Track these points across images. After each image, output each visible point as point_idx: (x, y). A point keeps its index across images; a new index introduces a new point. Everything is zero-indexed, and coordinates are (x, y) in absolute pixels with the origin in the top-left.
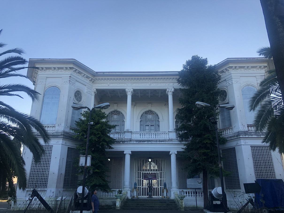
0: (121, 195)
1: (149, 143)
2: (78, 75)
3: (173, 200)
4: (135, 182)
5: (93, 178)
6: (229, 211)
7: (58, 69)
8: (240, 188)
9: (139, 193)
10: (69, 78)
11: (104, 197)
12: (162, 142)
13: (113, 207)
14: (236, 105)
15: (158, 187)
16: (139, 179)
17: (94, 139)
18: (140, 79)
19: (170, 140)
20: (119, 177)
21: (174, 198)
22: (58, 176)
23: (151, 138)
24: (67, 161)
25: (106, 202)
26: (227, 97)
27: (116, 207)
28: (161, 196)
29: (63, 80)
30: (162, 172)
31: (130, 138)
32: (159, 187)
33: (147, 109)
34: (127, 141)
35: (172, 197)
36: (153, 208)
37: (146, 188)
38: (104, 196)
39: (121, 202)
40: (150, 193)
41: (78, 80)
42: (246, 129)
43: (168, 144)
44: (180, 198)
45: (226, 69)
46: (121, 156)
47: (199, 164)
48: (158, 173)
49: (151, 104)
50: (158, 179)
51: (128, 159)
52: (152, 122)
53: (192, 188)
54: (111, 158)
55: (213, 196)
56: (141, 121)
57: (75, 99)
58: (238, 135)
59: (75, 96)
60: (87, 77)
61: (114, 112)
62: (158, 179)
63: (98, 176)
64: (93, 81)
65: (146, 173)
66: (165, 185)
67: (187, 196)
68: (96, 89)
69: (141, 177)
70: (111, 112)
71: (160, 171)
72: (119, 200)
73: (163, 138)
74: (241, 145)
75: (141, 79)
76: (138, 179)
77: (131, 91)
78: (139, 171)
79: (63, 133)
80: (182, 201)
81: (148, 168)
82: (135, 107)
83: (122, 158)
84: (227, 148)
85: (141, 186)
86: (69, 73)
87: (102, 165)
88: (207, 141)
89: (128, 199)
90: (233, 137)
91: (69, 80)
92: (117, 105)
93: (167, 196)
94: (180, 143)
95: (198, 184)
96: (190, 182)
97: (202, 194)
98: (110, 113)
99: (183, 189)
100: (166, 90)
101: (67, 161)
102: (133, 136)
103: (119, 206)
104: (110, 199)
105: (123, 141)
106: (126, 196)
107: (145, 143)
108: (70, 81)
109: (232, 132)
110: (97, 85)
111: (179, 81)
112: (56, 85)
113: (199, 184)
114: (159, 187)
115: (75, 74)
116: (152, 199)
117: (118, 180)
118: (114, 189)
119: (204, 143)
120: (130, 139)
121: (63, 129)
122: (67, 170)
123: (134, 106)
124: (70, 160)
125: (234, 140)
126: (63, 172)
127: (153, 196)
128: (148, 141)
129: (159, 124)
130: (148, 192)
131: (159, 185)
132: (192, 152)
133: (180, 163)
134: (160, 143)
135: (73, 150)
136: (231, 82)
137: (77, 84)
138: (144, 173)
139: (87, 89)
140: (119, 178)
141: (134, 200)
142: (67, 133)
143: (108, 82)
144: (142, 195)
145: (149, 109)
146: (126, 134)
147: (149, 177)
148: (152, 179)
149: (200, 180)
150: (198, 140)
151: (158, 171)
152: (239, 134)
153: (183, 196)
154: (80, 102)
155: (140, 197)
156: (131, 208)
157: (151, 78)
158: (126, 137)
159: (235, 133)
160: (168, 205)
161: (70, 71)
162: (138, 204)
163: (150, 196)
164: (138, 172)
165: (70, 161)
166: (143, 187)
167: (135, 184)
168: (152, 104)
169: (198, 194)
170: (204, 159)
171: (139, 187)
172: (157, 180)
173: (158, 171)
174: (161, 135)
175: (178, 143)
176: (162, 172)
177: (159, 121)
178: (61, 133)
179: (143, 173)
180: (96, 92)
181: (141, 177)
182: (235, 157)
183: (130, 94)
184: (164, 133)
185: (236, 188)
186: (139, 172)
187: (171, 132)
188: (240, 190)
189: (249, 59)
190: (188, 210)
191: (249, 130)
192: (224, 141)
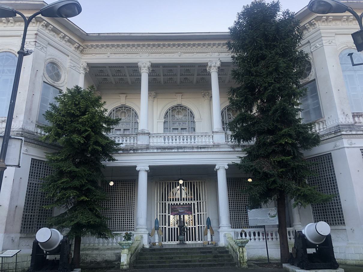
0: (130, 242)
1: (179, 151)
3: (223, 248)
4: (157, 219)
5: (77, 212)
6: (334, 265)
7: (15, 22)
8: (344, 223)
9: (163, 238)
10: (34, 36)
11: (95, 247)
12: (203, 150)
13: (116, 263)
14: (332, 83)
15: (195, 226)
16: (164, 214)
17: (77, 140)
18: (163, 46)
19: (215, 146)
20: (130, 211)
21: (225, 245)
22: (9, 211)
23: (183, 144)
24: (31, 183)
25: (105, 255)
26: (313, 70)
27: (121, 264)
28: (199, 240)
30: (200, 202)
31: (146, 143)
32: (197, 226)
33: (175, 104)
34: (142, 149)
35: (222, 243)
36: (190, 264)
37: (174, 228)
38: (101, 244)
39: (130, 255)
40: (181, 237)
42: (351, 121)
43: (211, 153)
44: (239, 245)
47: (274, 182)
48: (194, 204)
49: (181, 94)
50: (194, 213)
51: (143, 179)
52: (183, 123)
53: (257, 226)
54: (116, 182)
55: (306, 240)
56: (165, 122)
57: (47, 76)
58: (337, 132)
60: (70, 41)
61: (120, 108)
62: (194, 213)
63: (87, 208)
64: (82, 50)
65: (174, 204)
66: (209, 222)
67: (251, 239)
68: (87, 64)
69: (167, 211)
70: (116, 109)
71: (197, 200)
72: (126, 251)
73: (204, 144)
74: (344, 147)
75: (164, 45)
76: (161, 214)
77: (147, 66)
78: (162, 201)
79: (22, 131)
80: (242, 249)
81: (178, 196)
82: (156, 99)
83: (135, 181)
84: (310, 157)
85: (167, 227)
87: (93, 188)
88: (286, 141)
89: (143, 249)
90: (327, 135)
91: (35, 40)
92: (126, 97)
93: (212, 240)
94: (232, 150)
95: (271, 218)
96: (255, 216)
97: (276, 235)
98: (114, 111)
99: (235, 228)
101: (31, 183)
102: (151, 141)
103: (125, 263)
104: (111, 249)
105: (135, 148)
106: (140, 243)
107: (173, 151)
108: (36, 42)
109: (324, 128)
110: (89, 56)
111: (229, 46)
112: (11, 49)
113: (272, 218)
114: (197, 226)
115: (46, 32)
116: (186, 247)
117: (128, 217)
118: (118, 232)
119: (281, 144)
120: (147, 145)
121: (23, 126)
122: (30, 199)
123: (153, 97)
124: (35, 182)
125: (329, 140)
126: (21, 202)
127: (187, 242)
128: (178, 148)
129: (194, 126)
130: (179, 235)
131: (197, 223)
133: (230, 187)
134: (200, 150)
135: (42, 165)
136: (319, 44)
137: (51, 50)
138: (172, 204)
139: (70, 62)
140: (130, 213)
141: (154, 250)
142: (29, 134)
143: (108, 51)
144: (169, 241)
145: (179, 103)
146: (140, 137)
147: (179, 211)
148: (184, 214)
149: (274, 211)
150: (269, 139)
151: (194, 200)
152: (340, 130)
153: (245, 240)
154: (56, 82)
155: (166, 243)
156: (150, 266)
157: (182, 43)
158: (139, 143)
159: (330, 129)
160: (215, 257)
161: (37, 24)
162: (162, 258)
163: (182, 242)
164: (161, 202)
165: (37, 183)
166: (170, 227)
167: (157, 222)
168: (182, 96)
169: (270, 237)
170: (281, 172)
171: (163, 227)
172: (193, 214)
173: (194, 200)
174: (200, 139)
175: (230, 150)
176: (201, 201)
177: (194, 122)
178: (17, 133)
179: (169, 204)
180: (88, 70)
181: (167, 211)
182: (331, 170)
183: (146, 71)
184: (205, 135)
185: (333, 224)
186: (163, 203)
187: (217, 132)
188: (343, 227)
189: (350, 2)
190: (253, 264)
191: (356, 123)
192: (316, 140)
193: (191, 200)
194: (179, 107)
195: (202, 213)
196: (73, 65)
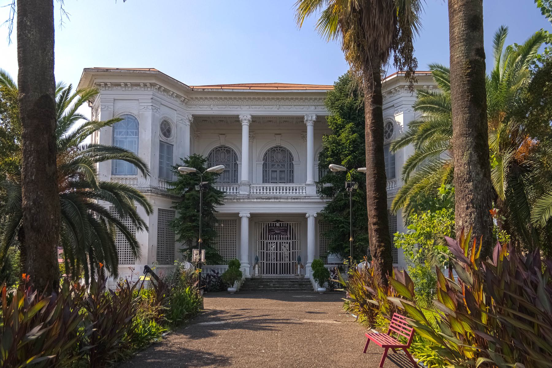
2: (164, 95)
10: (150, 101)
12: (296, 201)
16: (262, 251)
29: (141, 104)
33: (273, 145)
34: (244, 199)
41: (163, 102)
45: (395, 89)
46: (235, 219)
51: (245, 224)
57: (162, 135)
59: (162, 129)
66: (299, 259)
68: (193, 115)
85: (265, 262)
86: (150, 92)
94: (321, 201)
100: (303, 117)
107: (270, 201)
115: (160, 95)
132: (14, 248)
137: (164, 110)
141: (255, 279)
173: (290, 239)
175: (319, 201)
193: (287, 239)
194: (278, 149)
195: (296, 251)
196: (180, 119)
